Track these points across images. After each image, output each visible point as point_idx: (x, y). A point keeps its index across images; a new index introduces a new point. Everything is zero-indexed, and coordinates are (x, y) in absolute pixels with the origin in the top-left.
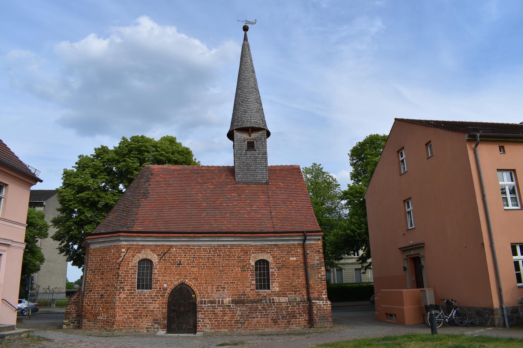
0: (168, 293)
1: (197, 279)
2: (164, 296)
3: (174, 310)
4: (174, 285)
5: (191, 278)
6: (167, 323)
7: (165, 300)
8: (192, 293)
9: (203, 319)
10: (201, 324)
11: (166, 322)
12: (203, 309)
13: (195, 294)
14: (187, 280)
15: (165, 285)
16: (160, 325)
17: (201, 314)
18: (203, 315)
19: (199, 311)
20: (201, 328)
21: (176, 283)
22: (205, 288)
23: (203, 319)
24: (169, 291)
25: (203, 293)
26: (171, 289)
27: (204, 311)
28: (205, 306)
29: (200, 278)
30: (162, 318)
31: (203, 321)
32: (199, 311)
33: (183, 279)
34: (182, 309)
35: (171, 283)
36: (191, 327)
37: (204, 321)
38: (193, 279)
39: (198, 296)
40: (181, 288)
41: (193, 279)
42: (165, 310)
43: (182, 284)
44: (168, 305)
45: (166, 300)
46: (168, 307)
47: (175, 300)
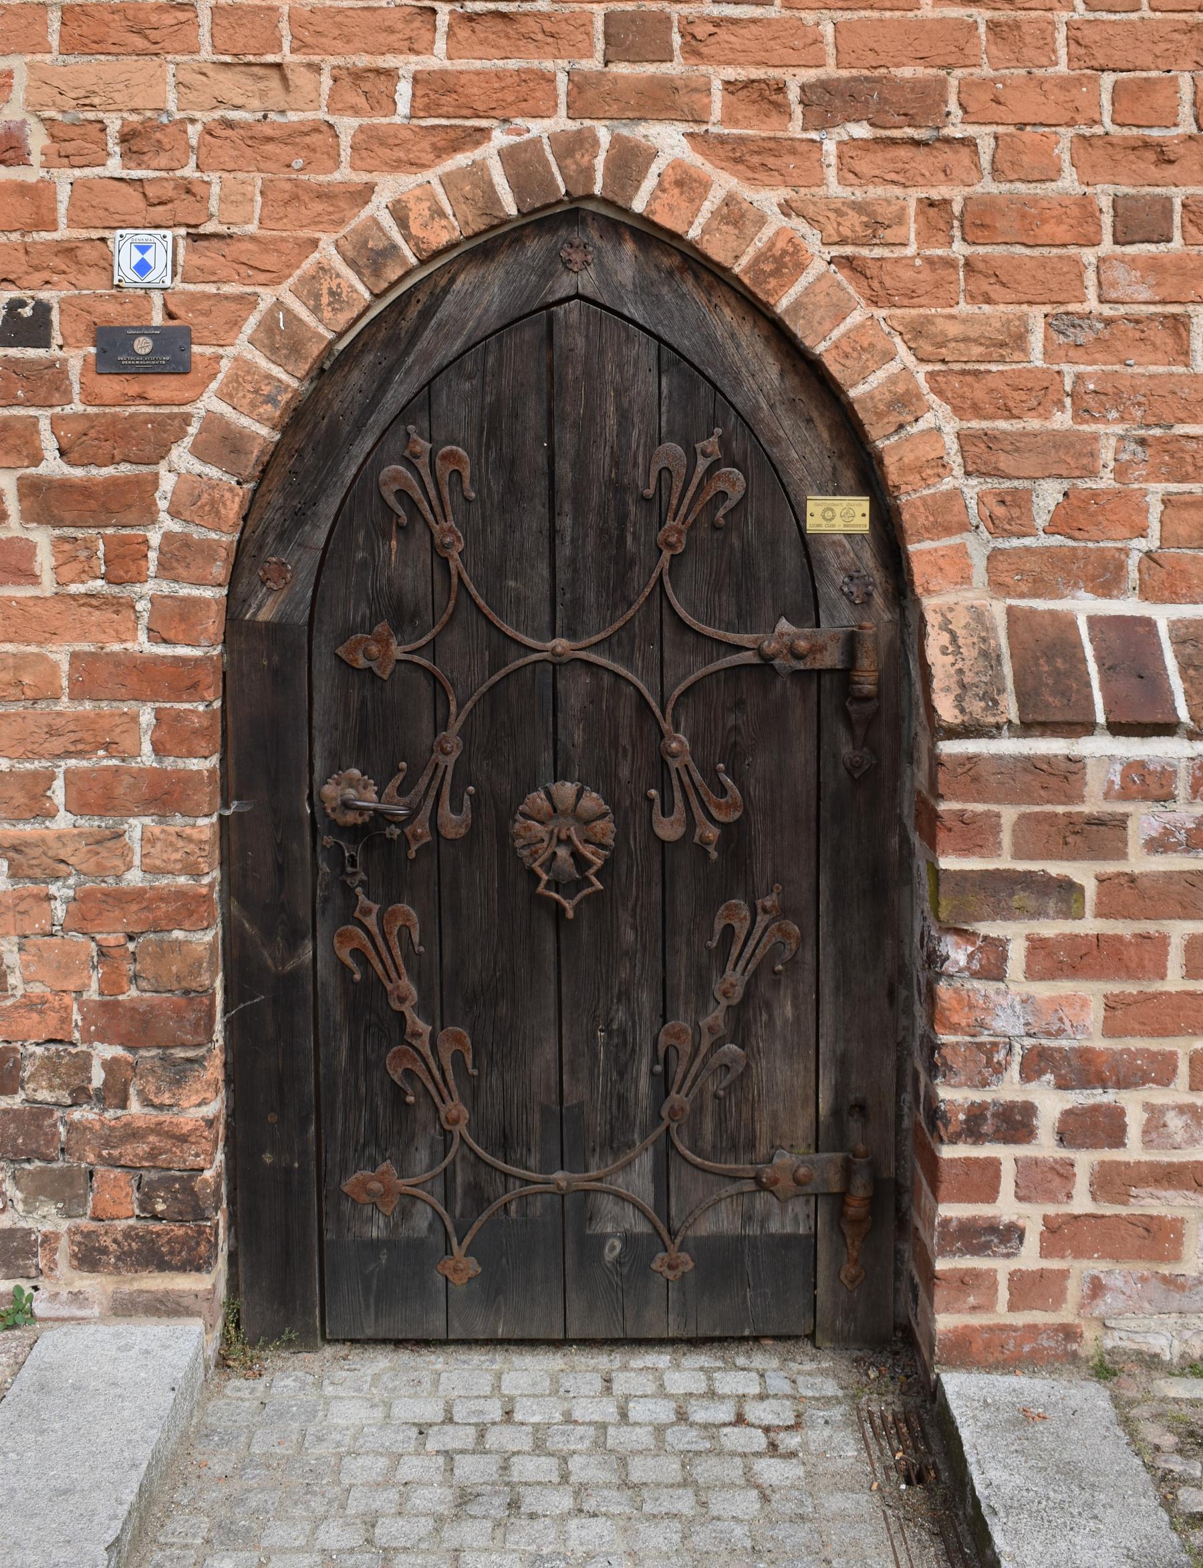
0: (222, 444)
1: (924, 102)
2: (132, 501)
3: (370, 833)
4: (370, 257)
5: (768, 96)
6: (242, 1131)
7: (173, 611)
8: (801, 444)
9: (1081, 1070)
10: (1042, 1181)
11: (203, 1105)
12: (1100, 835)
13: (865, 472)
14: (668, 140)
15: (146, 258)
16: (67, 1189)
17: (1050, 960)
18: (1090, 995)
19: (1000, 892)
20: (1029, 1288)
21: (420, 201)
22: (1109, 335)
23: (1081, 1070)
24: (240, 387)
25: (1074, 456)
26: (280, 338)
27: (1124, 895)
28: (1148, 784)
29: (986, 102)
30: (111, 1019)
31: (1084, 1128)
32: (1000, 892)
33: (586, 97)
34: (563, 819)
35: (288, 199)
36: (787, 1220)
37: (1096, 1128)
38: (826, 103)
39: (948, 517)
40: (535, 317)
41: (826, 103)
42: (174, 852)
43: (563, 218)
44: (297, 419)
45: (172, 619)
46: (231, 783)
47: (401, 617)
